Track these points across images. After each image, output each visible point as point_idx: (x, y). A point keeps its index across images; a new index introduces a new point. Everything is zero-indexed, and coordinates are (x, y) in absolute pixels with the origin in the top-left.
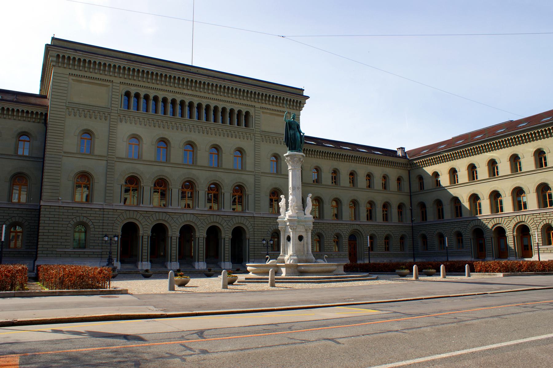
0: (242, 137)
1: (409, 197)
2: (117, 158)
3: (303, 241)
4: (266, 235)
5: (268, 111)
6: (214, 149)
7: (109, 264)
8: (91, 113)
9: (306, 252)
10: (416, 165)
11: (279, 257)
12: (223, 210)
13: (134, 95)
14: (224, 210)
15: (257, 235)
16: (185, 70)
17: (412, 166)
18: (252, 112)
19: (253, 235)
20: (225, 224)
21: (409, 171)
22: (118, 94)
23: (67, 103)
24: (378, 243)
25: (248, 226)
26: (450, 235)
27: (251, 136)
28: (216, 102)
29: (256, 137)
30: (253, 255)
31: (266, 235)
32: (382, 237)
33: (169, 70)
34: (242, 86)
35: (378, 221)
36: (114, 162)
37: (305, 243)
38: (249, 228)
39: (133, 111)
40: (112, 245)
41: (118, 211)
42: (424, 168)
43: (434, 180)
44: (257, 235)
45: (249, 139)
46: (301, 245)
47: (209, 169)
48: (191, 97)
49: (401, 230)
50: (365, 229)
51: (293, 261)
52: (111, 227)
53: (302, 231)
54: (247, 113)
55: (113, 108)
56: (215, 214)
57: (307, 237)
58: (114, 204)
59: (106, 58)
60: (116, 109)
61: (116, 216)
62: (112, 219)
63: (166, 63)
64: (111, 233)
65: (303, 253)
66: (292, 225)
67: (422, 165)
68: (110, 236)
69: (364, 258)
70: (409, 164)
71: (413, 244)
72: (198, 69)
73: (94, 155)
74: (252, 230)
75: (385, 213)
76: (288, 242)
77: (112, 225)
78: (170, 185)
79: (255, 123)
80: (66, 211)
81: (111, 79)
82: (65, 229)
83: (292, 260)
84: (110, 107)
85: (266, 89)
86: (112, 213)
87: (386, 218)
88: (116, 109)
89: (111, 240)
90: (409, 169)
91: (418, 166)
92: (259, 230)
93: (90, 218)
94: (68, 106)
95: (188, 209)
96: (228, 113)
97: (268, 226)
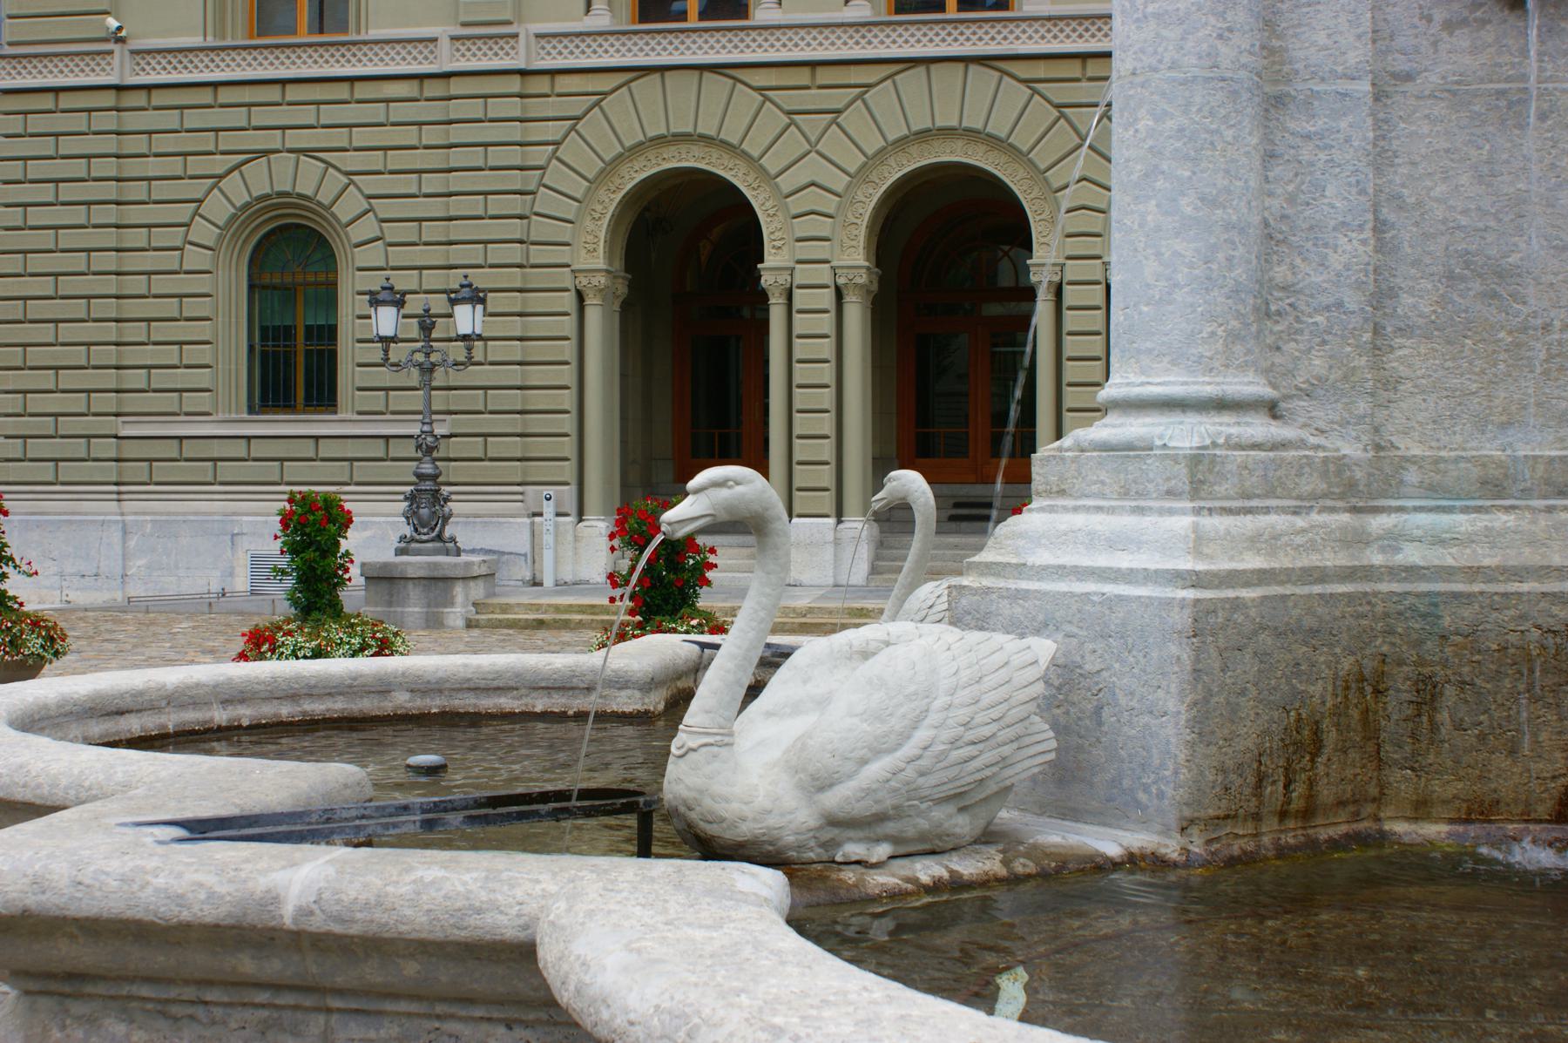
40: (439, 378)
52: (515, 229)
61: (553, 131)
62: (513, 156)
77: (516, 204)
82: (170, 260)
86: (512, 107)
93: (353, 161)
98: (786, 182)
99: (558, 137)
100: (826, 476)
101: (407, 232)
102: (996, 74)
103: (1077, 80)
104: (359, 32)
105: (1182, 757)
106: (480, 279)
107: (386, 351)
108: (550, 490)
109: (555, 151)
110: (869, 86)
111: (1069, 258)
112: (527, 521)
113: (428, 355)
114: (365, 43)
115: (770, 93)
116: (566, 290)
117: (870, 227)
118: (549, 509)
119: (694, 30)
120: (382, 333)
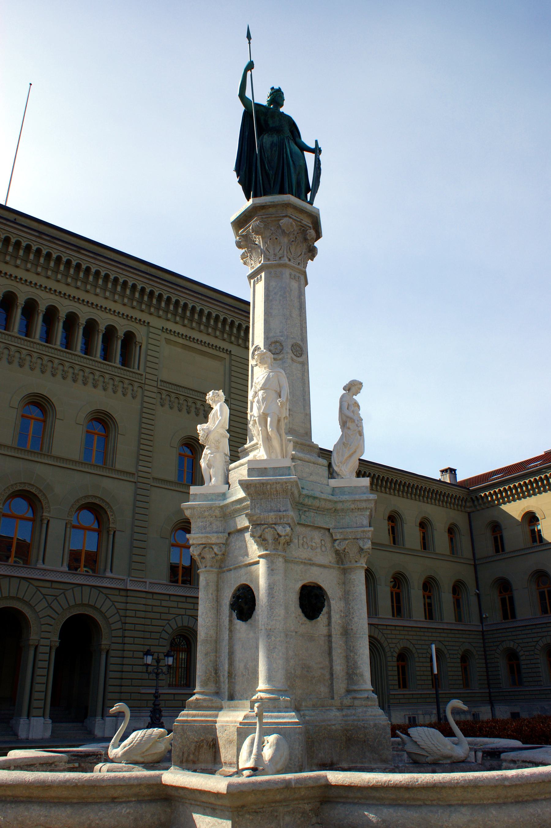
0: (110, 387)
1: (473, 567)
2: (154, 478)
3: (322, 618)
5: (180, 340)
6: (32, 407)
9: (340, 686)
10: (485, 500)
11: (185, 715)
12: (40, 565)
14: (43, 567)
15: (130, 640)
17: (476, 503)
18: (141, 333)
19: (120, 640)
20: (44, 604)
21: (469, 514)
24: (418, 669)
25: (108, 614)
26: (532, 653)
27: (135, 389)
28: (53, 297)
29: (146, 393)
32: (424, 655)
35: (414, 619)
36: (148, 487)
38: (111, 620)
42: (503, 507)
43: (527, 529)
44: (130, 640)
47: (13, 454)
49: (461, 640)
50: (389, 636)
51: (277, 745)
54: (129, 338)
56: (16, 574)
57: (347, 596)
65: (323, 690)
66: (271, 517)
67: (498, 499)
69: (389, 706)
70: (469, 499)
71: (487, 672)
74: (119, 625)
75: (427, 601)
76: (239, 625)
79: (146, 361)
81: (145, 317)
83: (272, 739)
84: (144, 374)
87: (429, 613)
90: (469, 510)
91: (490, 501)
92: (138, 627)
94: (160, 387)
96: (81, 328)
97: (164, 616)
102: (28, 583)
105: (300, 757)
107: (147, 668)
110: (67, 590)
113: (158, 670)
115: (39, 588)
119: (180, 586)
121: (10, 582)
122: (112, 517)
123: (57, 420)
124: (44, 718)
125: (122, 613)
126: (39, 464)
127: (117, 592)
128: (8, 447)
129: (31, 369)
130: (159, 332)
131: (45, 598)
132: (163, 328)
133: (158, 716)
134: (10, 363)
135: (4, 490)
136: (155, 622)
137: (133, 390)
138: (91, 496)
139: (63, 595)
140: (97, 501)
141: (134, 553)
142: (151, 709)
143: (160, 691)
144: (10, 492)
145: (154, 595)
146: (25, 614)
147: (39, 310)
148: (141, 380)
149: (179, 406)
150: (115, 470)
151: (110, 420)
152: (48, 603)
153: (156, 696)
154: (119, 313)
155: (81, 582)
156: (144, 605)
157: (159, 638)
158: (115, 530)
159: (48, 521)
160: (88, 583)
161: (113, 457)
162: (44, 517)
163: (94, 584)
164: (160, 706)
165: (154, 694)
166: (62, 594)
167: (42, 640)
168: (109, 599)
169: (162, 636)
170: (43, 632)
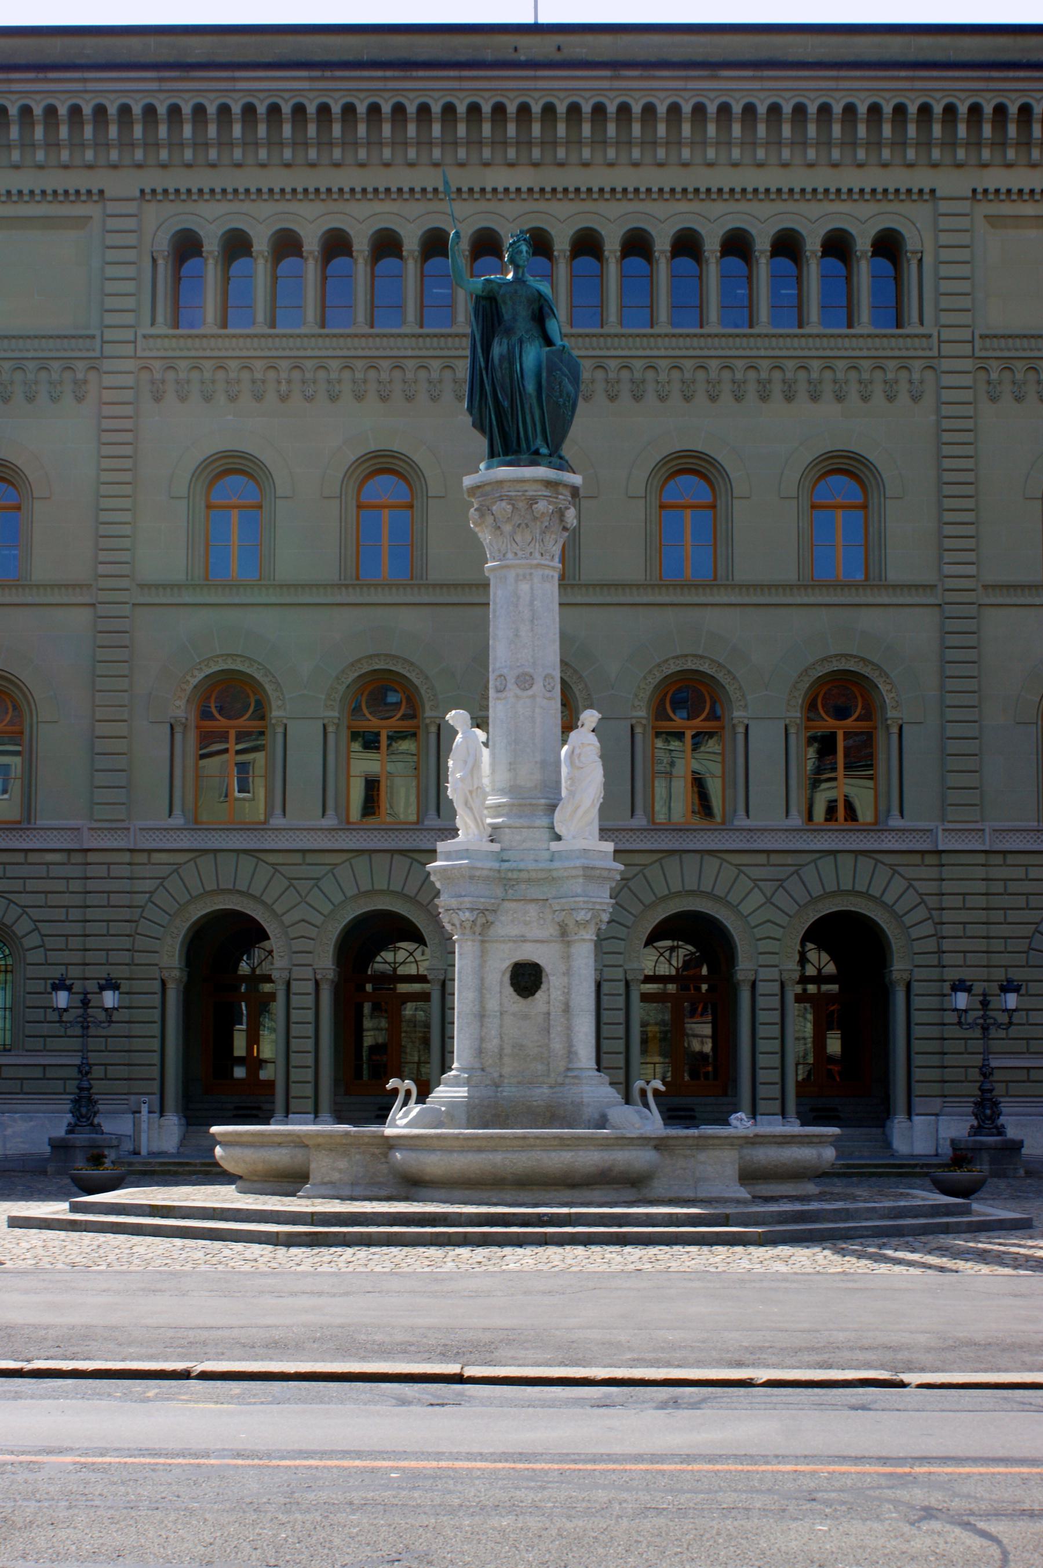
2: (985, 587)
4: (1021, 959)
7: (980, 1127)
8: (815, 375)
12: (741, 821)
13: (822, 246)
16: (489, 56)
22: (131, 255)
23: (139, 338)
25: (900, 908)
29: (947, 380)
30: (934, 1074)
31: (1021, 959)
33: (385, 79)
34: (832, 84)
36: (126, 610)
37: (556, 1010)
39: (618, 330)
40: (92, 1031)
41: (157, 857)
45: (904, 398)
46: (526, 1017)
48: (530, 206)
52: (126, 942)
53: (536, 932)
55: (109, 335)
56: (691, 846)
57: (482, 988)
58: (987, 826)
59: (654, 78)
60: (128, 335)
61: (149, 885)
62: (124, 899)
63: (945, 40)
64: (983, 973)
68: (978, 988)
72: (559, 39)
73: (887, 586)
77: (127, 928)
78: (428, 706)
80: (1020, 873)
81: (922, 179)
84: (98, 333)
85: (995, 74)
88: (128, 335)
89: (85, 1003)
93: (24, 899)
94: (984, 354)
95: (851, 825)
98: (287, 919)
99: (152, 889)
100: (309, 1091)
101: (60, 943)
102: (255, 860)
103: (300, 864)
104: (29, 823)
106: (1016, 974)
108: (144, 1098)
109: (150, 897)
111: (761, 966)
112: (131, 1116)
114: (35, 829)
115: (278, 867)
116: (155, 979)
117: (335, 946)
118: (144, 1109)
120: (1009, 1007)
121: (681, 862)
122: (892, 695)
123: (735, 502)
124: (784, 1118)
125: (932, 902)
126: (709, 608)
127: (917, 859)
128: (638, 586)
129: (736, 400)
130: (964, 206)
131: (757, 886)
132: (9, 192)
133: (988, 1112)
134: (612, 398)
135: (645, 678)
136: (1012, 916)
137: (910, 382)
138: (836, 656)
139: (795, 876)
140: (851, 666)
141: (950, 768)
142: (72, 1097)
143: (994, 1063)
144: (658, 680)
145: (1009, 856)
146: (721, 923)
147: (906, 252)
148: (930, 349)
149: (786, 388)
150: (887, 587)
151: (864, 469)
152: (766, 897)
153: (986, 1072)
154: (20, 192)
155: (833, 846)
156: (983, 880)
157: (1026, 949)
158: (900, 722)
159: (747, 727)
160: (848, 847)
161: (880, 556)
162: (735, 721)
163: (862, 846)
164: (994, 1093)
165: (79, 1066)
166: (792, 874)
167: (761, 969)
168: (745, 874)
169: (1033, 946)
170: (761, 953)
